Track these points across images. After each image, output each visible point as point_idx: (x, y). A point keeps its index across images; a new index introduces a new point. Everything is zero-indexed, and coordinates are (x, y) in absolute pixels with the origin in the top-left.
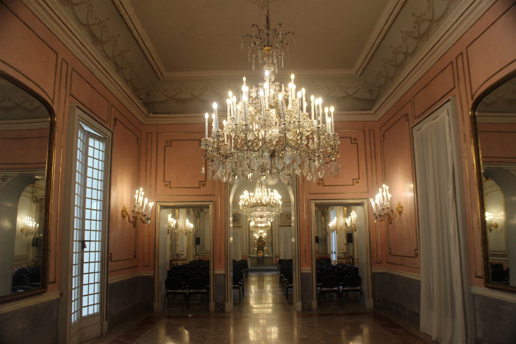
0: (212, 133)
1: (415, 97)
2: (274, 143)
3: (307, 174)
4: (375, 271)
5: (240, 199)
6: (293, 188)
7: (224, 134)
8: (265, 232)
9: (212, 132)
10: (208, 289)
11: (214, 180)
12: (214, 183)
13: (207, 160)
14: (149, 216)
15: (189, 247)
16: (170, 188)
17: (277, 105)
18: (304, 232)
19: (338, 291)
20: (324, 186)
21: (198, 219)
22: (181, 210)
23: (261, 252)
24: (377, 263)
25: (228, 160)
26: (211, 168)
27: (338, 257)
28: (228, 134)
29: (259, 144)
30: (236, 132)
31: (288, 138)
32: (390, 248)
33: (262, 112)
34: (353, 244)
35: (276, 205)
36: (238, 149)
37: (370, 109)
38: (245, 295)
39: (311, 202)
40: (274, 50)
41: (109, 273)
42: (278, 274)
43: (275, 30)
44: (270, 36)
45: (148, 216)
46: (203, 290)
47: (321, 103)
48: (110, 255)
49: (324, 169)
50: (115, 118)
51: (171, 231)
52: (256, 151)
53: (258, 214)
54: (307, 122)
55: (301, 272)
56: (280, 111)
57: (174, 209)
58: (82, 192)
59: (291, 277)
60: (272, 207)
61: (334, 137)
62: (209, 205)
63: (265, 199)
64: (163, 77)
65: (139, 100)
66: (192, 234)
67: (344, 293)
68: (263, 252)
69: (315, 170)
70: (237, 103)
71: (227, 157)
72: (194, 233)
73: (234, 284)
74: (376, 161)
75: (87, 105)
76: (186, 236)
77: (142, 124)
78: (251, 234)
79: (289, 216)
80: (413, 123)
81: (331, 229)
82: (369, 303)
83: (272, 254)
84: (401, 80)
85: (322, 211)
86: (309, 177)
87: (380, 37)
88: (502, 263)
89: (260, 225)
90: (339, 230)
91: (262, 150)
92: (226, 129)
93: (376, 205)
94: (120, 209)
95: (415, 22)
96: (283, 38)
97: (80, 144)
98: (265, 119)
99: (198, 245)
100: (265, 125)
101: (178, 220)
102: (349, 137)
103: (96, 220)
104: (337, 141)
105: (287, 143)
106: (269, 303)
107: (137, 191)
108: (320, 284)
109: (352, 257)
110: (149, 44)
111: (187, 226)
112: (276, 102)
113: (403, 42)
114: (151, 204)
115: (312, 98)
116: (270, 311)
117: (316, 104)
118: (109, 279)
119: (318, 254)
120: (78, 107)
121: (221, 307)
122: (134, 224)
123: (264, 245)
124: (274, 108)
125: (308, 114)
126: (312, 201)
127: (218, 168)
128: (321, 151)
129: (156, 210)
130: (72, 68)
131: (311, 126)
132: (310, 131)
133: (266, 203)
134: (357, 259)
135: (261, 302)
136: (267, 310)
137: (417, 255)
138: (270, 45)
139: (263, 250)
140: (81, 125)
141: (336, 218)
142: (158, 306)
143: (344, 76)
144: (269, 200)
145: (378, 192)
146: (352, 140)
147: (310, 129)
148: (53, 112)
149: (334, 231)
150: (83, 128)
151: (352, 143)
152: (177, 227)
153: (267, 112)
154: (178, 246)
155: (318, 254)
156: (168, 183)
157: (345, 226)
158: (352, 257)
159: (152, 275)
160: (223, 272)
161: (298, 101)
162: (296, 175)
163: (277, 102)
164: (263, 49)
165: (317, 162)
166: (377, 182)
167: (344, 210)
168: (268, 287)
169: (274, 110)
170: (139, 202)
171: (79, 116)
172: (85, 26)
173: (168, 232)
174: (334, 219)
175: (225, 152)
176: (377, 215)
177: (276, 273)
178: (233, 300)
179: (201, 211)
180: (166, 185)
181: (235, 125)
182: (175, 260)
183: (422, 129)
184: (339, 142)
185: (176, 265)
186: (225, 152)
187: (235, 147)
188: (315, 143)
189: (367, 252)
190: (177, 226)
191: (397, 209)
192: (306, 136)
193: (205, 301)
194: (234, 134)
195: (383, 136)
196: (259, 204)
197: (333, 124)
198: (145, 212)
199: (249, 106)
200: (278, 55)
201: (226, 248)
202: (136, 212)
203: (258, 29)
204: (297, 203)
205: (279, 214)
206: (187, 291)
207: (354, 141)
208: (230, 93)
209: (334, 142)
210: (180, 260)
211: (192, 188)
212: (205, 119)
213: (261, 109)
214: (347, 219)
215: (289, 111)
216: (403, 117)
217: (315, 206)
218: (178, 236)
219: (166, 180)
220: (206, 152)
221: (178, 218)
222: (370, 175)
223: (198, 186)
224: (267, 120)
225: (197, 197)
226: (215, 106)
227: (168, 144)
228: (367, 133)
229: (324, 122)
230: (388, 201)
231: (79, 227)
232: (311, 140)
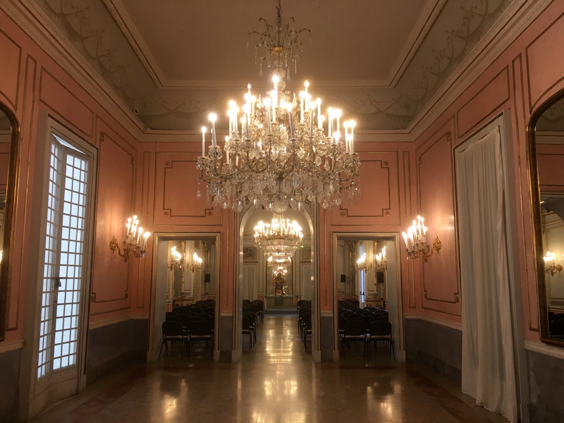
1: (459, 112)
8: (285, 268)
12: (222, 212)
16: (171, 216)
17: (288, 119)
20: (348, 216)
21: (209, 253)
24: (410, 307)
30: (236, 149)
32: (425, 291)
34: (384, 285)
35: (295, 238)
37: (405, 128)
39: (333, 234)
40: (285, 51)
41: (90, 317)
43: (288, 26)
44: (281, 34)
50: (101, 132)
51: (175, 266)
52: (260, 172)
57: (180, 241)
58: (57, 220)
60: (290, 240)
61: (353, 157)
62: (216, 236)
66: (200, 270)
67: (372, 343)
73: (243, 329)
74: (410, 189)
76: (193, 272)
77: (138, 141)
80: (455, 144)
82: (401, 355)
83: (293, 294)
85: (350, 246)
88: (553, 311)
89: (278, 261)
90: (369, 268)
93: (409, 240)
94: (108, 240)
96: (297, 36)
97: (53, 161)
98: (270, 134)
100: (272, 140)
101: (184, 254)
118: (90, 323)
120: (49, 115)
121: (227, 357)
122: (126, 257)
126: (334, 233)
130: (42, 67)
135: (279, 350)
136: (286, 360)
137: (457, 300)
140: (55, 138)
142: (152, 355)
146: (383, 164)
148: (16, 120)
149: (363, 269)
150: (59, 142)
151: (382, 168)
153: (274, 126)
154: (183, 284)
156: (169, 211)
157: (375, 263)
158: (382, 299)
159: (147, 317)
164: (273, 50)
165: (331, 187)
168: (288, 333)
170: (132, 232)
176: (409, 251)
177: (295, 316)
179: (212, 244)
180: (166, 214)
181: (235, 140)
183: (466, 150)
184: (359, 163)
185: (180, 305)
190: (182, 261)
191: (434, 244)
193: (210, 349)
195: (420, 158)
197: (352, 142)
201: (235, 285)
203: (267, 24)
206: (188, 337)
207: (384, 165)
210: (186, 300)
214: (377, 256)
215: (301, 125)
218: (183, 272)
221: (185, 252)
224: (273, 135)
228: (401, 155)
231: (52, 261)
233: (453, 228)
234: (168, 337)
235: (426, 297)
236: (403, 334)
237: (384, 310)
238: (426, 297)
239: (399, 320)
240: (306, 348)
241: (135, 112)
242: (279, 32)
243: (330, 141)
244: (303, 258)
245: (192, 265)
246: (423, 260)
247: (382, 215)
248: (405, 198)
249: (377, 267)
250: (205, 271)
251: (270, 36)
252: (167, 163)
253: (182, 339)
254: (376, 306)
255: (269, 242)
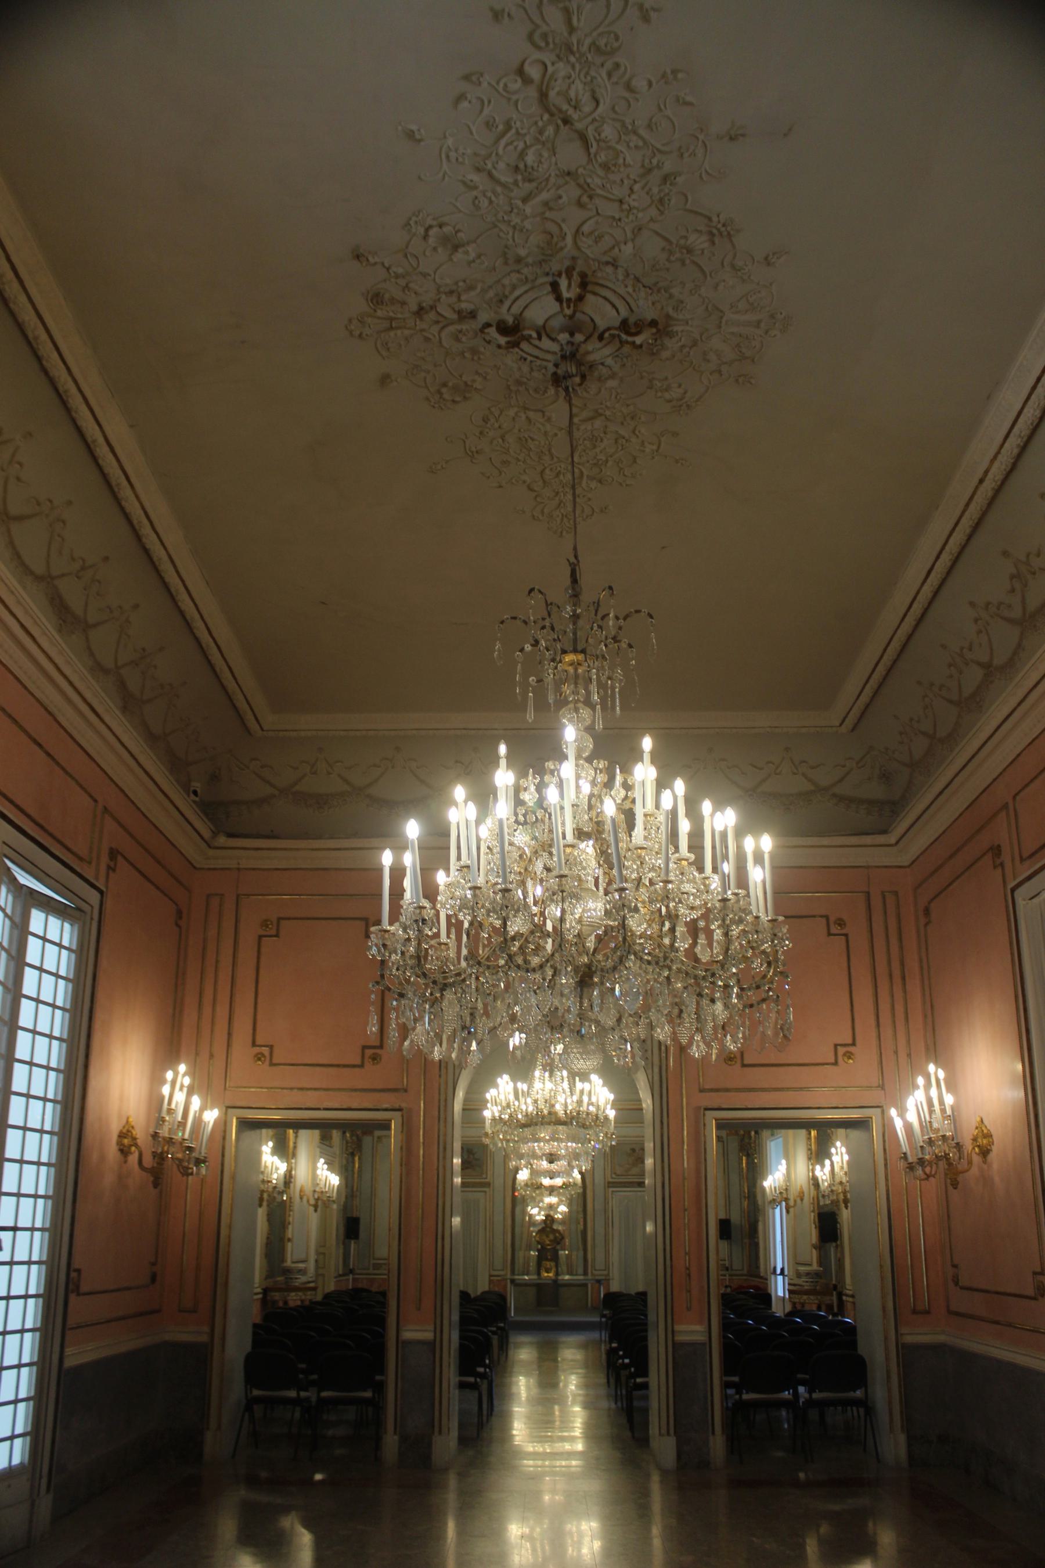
0: (402, 911)
1: (1018, 798)
2: (591, 943)
3: (692, 1038)
4: (909, 1339)
5: (487, 1101)
6: (649, 1071)
7: (438, 912)
8: (563, 1201)
9: (402, 907)
10: (380, 1388)
11: (405, 1053)
13: (387, 992)
14: (203, 1151)
15: (324, 1246)
16: (272, 1064)
17: (600, 829)
18: (685, 1210)
19: (790, 1405)
20: (744, 1066)
21: (357, 1159)
22: (303, 1133)
23: (548, 1266)
24: (915, 1312)
25: (449, 995)
26: (397, 1017)
27: (792, 1288)
28: (450, 912)
29: (544, 948)
31: (631, 931)
32: (955, 1266)
33: (554, 851)
34: (840, 1248)
35: (598, 1121)
36: (479, 963)
37: (884, 832)
38: (496, 1409)
39: (704, 1115)
40: (592, 665)
41: (68, 1333)
42: (603, 1338)
43: (597, 605)
44: (581, 623)
45: (200, 1153)
46: (365, 1390)
47: (733, 825)
48: (74, 1275)
49: (743, 1025)
51: (269, 1196)
53: (540, 1148)
54: (689, 881)
55: (673, 1340)
56: (608, 847)
59: (644, 1351)
60: (584, 1126)
61: (772, 929)
63: (564, 1102)
64: (262, 730)
65: (189, 796)
66: (335, 1206)
68: (557, 1266)
69: (715, 1028)
70: (478, 822)
71: (445, 985)
72: (342, 1203)
74: (905, 991)
75: (30, 811)
76: (316, 1211)
77: (195, 868)
78: (518, 1210)
79: (636, 1155)
80: (1015, 878)
81: (770, 1198)
83: (585, 1273)
84: (976, 744)
85: (742, 1140)
86: (698, 1046)
87: (910, 620)
89: (546, 1182)
90: (795, 1201)
91: (551, 966)
92: (444, 899)
93: (908, 1127)
94: (115, 1127)
95: (1012, 577)
96: (620, 628)
98: (562, 872)
99: (353, 1242)
101: (293, 1161)
102: (821, 916)
103: (38, 1164)
104: (782, 939)
105: (630, 946)
106: (572, 1439)
107: (169, 1075)
108: (736, 1379)
109: (838, 1289)
110: (223, 632)
111: (320, 1180)
112: (597, 818)
113: (979, 632)
114: (211, 1116)
115: (707, 806)
116: (576, 1466)
117: (719, 827)
118: (68, 1351)
119: (730, 1275)
123: (558, 1243)
124: (590, 838)
125: (692, 857)
126: (707, 1113)
127: (416, 1020)
128: (734, 970)
129: (225, 1131)
131: (702, 892)
132: (700, 907)
133: (566, 1111)
134: (853, 1296)
138: (579, 648)
139: (555, 1258)
140: (9, 869)
141: (784, 1162)
143: (804, 730)
144: (575, 1105)
145: (916, 1087)
147: (700, 901)
149: (780, 1203)
150: (15, 879)
151: (829, 934)
152: (290, 1182)
153: (568, 850)
154: (289, 1244)
155: (730, 1275)
156: (266, 1051)
157: (812, 1187)
158: (835, 1287)
159: (204, 1338)
160: (429, 1336)
161: (661, 818)
162: (660, 1043)
163: (600, 819)
164: (560, 662)
165: (719, 1006)
166: (909, 1055)
167: (809, 1138)
168: (572, 1384)
169: (591, 843)
170: (173, 1106)
171: (4, 843)
172: (39, 579)
173: (261, 1199)
174: (780, 1167)
175: (442, 967)
176: (910, 1160)
177: (595, 1335)
178: (456, 1424)
180: (259, 1057)
182: (279, 1290)
185: (281, 1304)
186: (442, 967)
187: (472, 956)
188: (715, 944)
189: (882, 1278)
190: (288, 1179)
191: (975, 1140)
192: (686, 923)
194: (467, 917)
195: (927, 911)
196: (543, 1117)
198: (191, 1139)
199: (515, 830)
200: (603, 679)
202: (164, 1138)
203: (546, 601)
204: (662, 1117)
205: (608, 1149)
208: (459, 792)
209: (772, 942)
210: (297, 1289)
211: (338, 1066)
212: (380, 870)
213: (552, 840)
216: (985, 854)
217: (719, 1127)
219: (259, 1042)
220: (383, 969)
221: (294, 1155)
222: (887, 1032)
223: (358, 1062)
225: (354, 1094)
226: (413, 829)
227: (271, 929)
228: (876, 902)
229: (742, 880)
230: (946, 1117)
232: (703, 936)
233: (1022, 1094)
234: (256, 1392)
235: (956, 1283)
236: (900, 1386)
237: (840, 1318)
238: (956, 1283)
239: (887, 1348)
240: (632, 1428)
241: (192, 796)
242: (575, 617)
243: (709, 885)
244: (615, 1173)
245: (315, 1191)
246: (946, 1181)
247: (833, 1061)
248: (894, 1015)
249: (821, 1198)
250: (345, 1208)
251: (553, 629)
252: (265, 924)
253: (296, 1402)
254: (819, 1308)
255: (527, 1132)
